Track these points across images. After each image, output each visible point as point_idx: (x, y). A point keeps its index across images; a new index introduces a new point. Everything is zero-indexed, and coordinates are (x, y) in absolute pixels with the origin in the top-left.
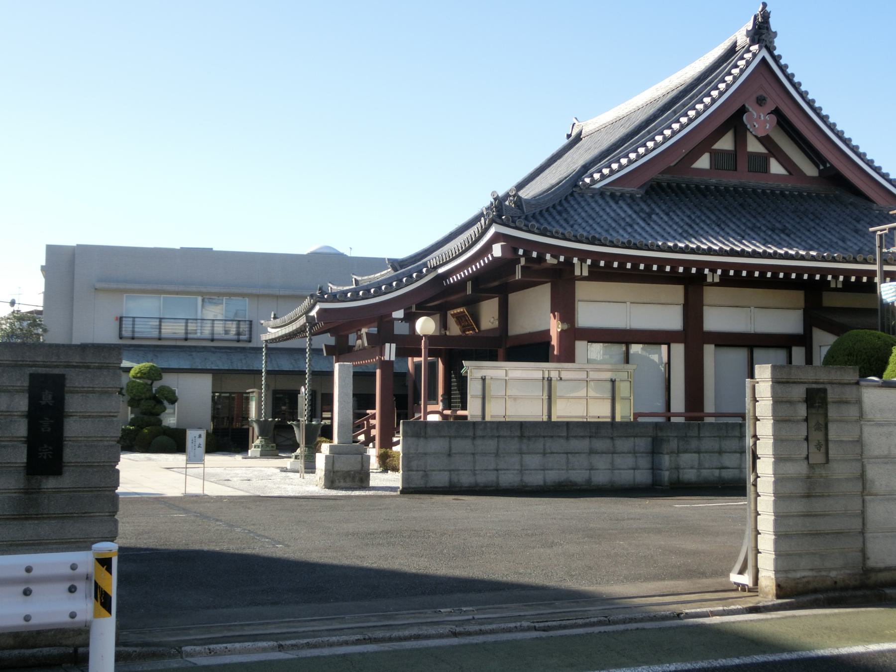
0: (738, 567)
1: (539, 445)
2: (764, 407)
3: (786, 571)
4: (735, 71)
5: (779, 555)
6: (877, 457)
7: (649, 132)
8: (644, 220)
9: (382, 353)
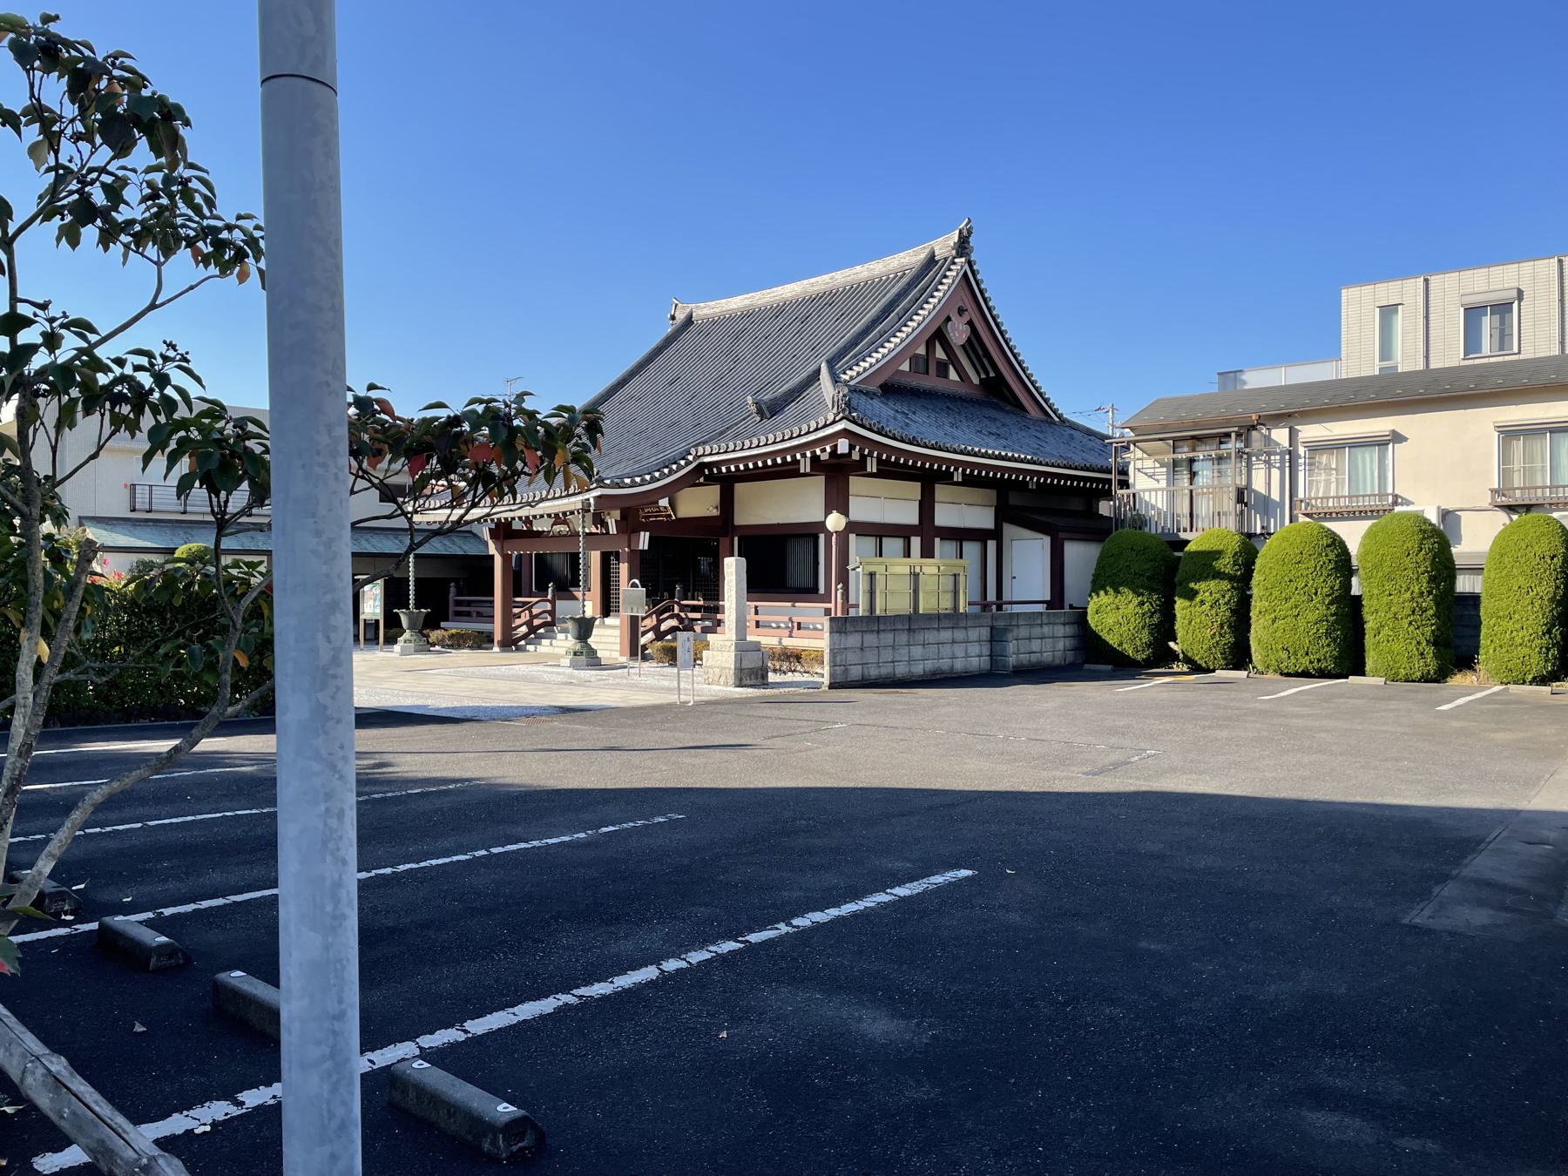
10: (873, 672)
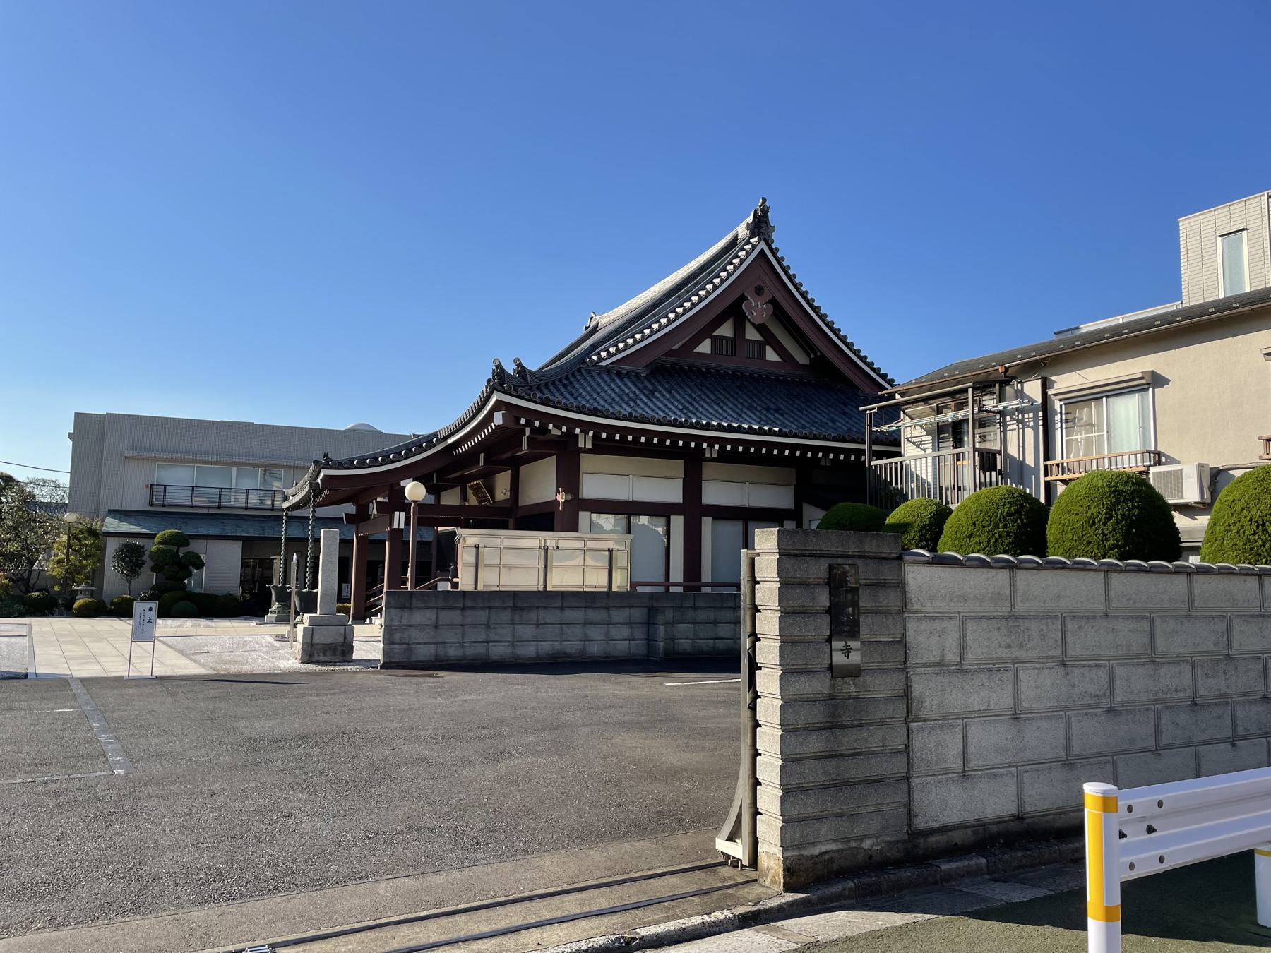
0: (727, 829)
1: (533, 616)
2: (768, 592)
3: (800, 847)
4: (736, 261)
5: (789, 821)
6: (925, 665)
7: (654, 315)
8: (647, 396)
9: (391, 523)
10: (453, 652)
